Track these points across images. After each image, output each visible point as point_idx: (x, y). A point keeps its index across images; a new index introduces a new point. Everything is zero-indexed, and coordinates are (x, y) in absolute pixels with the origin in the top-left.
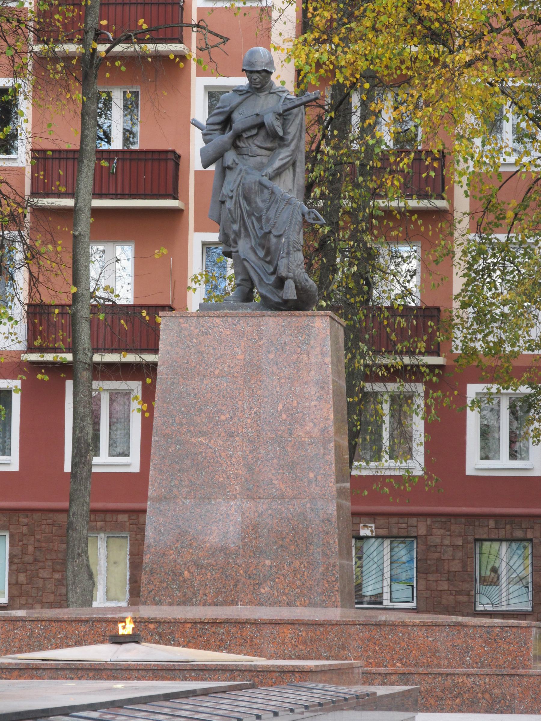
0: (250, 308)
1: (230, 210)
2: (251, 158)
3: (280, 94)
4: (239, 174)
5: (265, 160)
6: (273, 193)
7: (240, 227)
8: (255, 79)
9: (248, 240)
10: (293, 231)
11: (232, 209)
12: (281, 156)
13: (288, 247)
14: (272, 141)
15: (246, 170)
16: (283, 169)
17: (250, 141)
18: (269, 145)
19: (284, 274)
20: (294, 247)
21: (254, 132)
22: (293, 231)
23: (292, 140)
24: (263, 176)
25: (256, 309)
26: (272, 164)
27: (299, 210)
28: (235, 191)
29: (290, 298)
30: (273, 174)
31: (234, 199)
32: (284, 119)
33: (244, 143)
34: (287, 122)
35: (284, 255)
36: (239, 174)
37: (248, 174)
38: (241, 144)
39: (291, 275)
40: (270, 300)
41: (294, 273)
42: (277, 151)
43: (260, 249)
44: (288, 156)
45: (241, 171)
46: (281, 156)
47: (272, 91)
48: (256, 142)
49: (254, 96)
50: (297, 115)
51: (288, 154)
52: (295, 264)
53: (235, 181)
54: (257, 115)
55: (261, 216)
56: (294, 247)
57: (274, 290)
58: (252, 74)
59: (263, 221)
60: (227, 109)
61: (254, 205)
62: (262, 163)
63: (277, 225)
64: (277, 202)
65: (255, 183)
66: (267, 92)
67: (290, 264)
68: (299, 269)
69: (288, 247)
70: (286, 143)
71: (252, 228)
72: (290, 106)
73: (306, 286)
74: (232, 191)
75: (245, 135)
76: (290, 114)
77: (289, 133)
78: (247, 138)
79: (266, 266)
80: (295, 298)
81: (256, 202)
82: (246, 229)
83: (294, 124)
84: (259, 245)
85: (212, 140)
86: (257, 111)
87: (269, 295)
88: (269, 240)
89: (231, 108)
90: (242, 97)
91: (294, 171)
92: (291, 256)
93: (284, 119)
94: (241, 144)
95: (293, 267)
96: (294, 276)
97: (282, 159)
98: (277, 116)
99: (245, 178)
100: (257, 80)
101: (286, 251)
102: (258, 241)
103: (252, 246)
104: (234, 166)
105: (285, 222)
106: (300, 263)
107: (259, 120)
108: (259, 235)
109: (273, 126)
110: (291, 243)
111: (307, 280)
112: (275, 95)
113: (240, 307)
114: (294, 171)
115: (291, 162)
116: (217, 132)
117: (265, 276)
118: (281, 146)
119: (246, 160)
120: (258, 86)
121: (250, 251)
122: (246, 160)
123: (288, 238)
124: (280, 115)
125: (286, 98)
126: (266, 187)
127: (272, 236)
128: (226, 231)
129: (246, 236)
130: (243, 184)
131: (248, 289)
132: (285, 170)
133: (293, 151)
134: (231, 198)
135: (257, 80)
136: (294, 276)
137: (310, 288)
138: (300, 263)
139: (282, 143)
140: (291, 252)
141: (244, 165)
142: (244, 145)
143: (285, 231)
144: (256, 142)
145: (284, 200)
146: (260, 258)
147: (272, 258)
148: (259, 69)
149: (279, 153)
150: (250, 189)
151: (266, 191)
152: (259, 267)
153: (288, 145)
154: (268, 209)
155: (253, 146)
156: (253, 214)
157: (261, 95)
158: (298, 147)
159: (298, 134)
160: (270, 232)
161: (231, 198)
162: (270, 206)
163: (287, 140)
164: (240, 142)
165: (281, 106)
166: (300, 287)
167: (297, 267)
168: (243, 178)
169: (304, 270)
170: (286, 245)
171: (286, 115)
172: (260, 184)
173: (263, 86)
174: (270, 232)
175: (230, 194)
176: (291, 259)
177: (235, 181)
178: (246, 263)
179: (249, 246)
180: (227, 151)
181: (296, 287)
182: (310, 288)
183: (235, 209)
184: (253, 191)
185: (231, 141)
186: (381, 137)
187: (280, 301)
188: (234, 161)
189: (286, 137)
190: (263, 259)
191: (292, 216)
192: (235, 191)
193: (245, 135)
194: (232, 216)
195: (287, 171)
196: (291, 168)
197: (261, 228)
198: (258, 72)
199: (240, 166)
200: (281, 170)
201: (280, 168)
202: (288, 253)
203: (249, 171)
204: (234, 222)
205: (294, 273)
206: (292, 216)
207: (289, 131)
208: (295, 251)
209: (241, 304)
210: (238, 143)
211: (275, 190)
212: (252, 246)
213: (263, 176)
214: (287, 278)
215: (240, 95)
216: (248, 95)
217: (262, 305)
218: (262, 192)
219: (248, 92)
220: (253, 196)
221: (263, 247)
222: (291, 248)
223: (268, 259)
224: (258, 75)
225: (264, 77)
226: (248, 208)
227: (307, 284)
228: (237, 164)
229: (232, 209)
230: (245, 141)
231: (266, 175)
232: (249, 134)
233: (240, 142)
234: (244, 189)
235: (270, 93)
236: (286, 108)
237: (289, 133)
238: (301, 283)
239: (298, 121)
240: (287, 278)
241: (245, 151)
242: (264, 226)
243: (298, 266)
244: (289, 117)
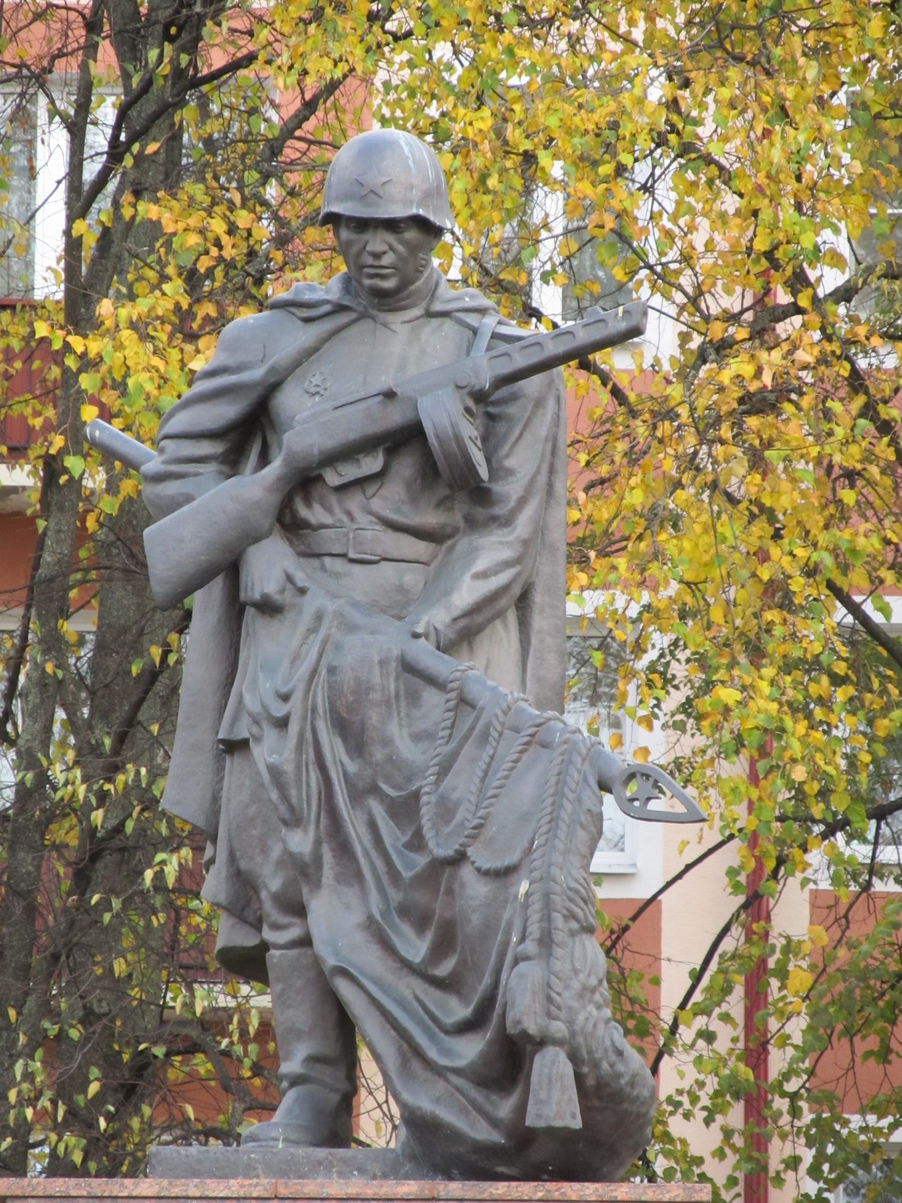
0: (362, 1171)
1: (275, 772)
2: (358, 569)
3: (472, 319)
4: (313, 630)
5: (412, 577)
6: (464, 702)
7: (318, 843)
8: (377, 256)
9: (351, 894)
10: (567, 852)
11: (289, 767)
12: (480, 565)
13: (547, 918)
14: (439, 504)
15: (339, 614)
16: (487, 613)
17: (354, 502)
18: (431, 519)
19: (532, 1027)
20: (571, 916)
21: (372, 464)
22: (567, 852)
23: (522, 502)
24: (416, 636)
25: (385, 1176)
26: (448, 593)
27: (586, 768)
28: (297, 697)
29: (558, 1123)
30: (452, 636)
31: (294, 728)
32: (491, 417)
33: (329, 510)
34: (501, 428)
35: (530, 947)
36: (313, 630)
37: (350, 628)
38: (314, 514)
39: (558, 1028)
40: (456, 1136)
41: (570, 1023)
42: (462, 544)
43: (407, 929)
44: (507, 564)
45: (319, 617)
46: (480, 565)
47: (437, 307)
48: (377, 505)
49: (365, 326)
50: (539, 403)
51: (507, 554)
52: (576, 985)
53: (295, 659)
54: (390, 395)
55: (416, 796)
56: (571, 916)
57: (475, 1093)
58: (368, 236)
59: (426, 813)
60: (256, 374)
61: (379, 754)
62: (401, 589)
63: (491, 830)
64: (485, 737)
65: (383, 663)
66: (416, 312)
67: (557, 985)
68: (591, 1008)
69: (547, 918)
70: (497, 510)
71: (369, 845)
72: (520, 361)
73: (619, 1076)
74: (285, 698)
75: (332, 478)
76: (513, 398)
77: (511, 472)
78: (341, 489)
79: (431, 996)
80: (577, 1123)
81: (387, 742)
82: (344, 849)
83: (528, 436)
84: (404, 911)
85: (189, 499)
86: (385, 381)
87: (447, 1116)
88: (450, 892)
89: (272, 370)
90: (307, 335)
91: (524, 624)
92: (558, 952)
93: (491, 417)
94: (314, 514)
95: (567, 998)
96: (573, 1034)
97: (484, 575)
98: (470, 403)
99: (338, 647)
100: (387, 260)
101: (534, 930)
102: (395, 896)
103: (370, 918)
104: (288, 597)
105: (525, 818)
106: (593, 981)
107: (395, 417)
108: (406, 874)
109: (458, 438)
110: (557, 900)
111: (620, 1053)
112: (448, 324)
113: (316, 1168)
114: (524, 624)
115: (516, 591)
116: (210, 469)
117: (432, 1037)
118: (472, 524)
119: (337, 576)
120: (389, 284)
121: (360, 937)
122: (337, 576)
123: (546, 878)
124: (480, 397)
125: (495, 336)
126: (432, 681)
127: (467, 873)
128: (243, 865)
129: (340, 879)
130: (332, 670)
131: (335, 1098)
132: (491, 620)
133: (526, 543)
134: (282, 723)
135: (387, 260)
136: (573, 1034)
137: (632, 1084)
138: (593, 981)
139: (481, 513)
140: (560, 936)
141: (335, 596)
142: (327, 519)
143: (529, 851)
144: (377, 505)
145: (517, 730)
146: (406, 965)
147: (462, 962)
148: (398, 211)
149: (473, 552)
150: (362, 689)
151: (431, 697)
152: (402, 1003)
153: (507, 521)
154: (445, 768)
155: (363, 519)
156: (374, 790)
157: (396, 319)
158: (540, 529)
159: (542, 479)
160: (461, 857)
161: (282, 723)
162: (453, 757)
163: (502, 500)
164: (308, 503)
165: (484, 363)
166: (590, 1082)
167: (581, 996)
168: (329, 647)
169: (608, 1012)
170: (536, 906)
171: (497, 403)
172: (408, 667)
173: (404, 285)
174: (461, 857)
175: (279, 710)
176: (557, 965)
177: (295, 659)
178: (344, 988)
179: (357, 917)
180: (255, 538)
181: (579, 1078)
182: (632, 1084)
183: (298, 767)
184: (376, 696)
185: (275, 500)
186: (357, 679)
187: (496, 1137)
188: (290, 579)
189: (497, 488)
190: (420, 973)
191: (559, 794)
192: (297, 697)
193: (332, 478)
194: (284, 797)
195: (498, 623)
196: (512, 616)
197: (417, 843)
198: (391, 225)
199: (309, 605)
200: (479, 619)
201: (476, 608)
202: (546, 941)
203: (358, 618)
204: (294, 820)
205: (570, 1023)
206: (559, 794)
207: (510, 463)
208: (572, 934)
209: (322, 1153)
210: (303, 512)
211: (474, 691)
212: (370, 918)
213: (416, 636)
214: (541, 1043)
215: (307, 320)
216: (343, 318)
217: (413, 1158)
218: (414, 698)
219: (340, 308)
220: (374, 717)
221: (421, 922)
222: (558, 920)
223: (444, 969)
224: (390, 238)
225: (414, 249)
226: (352, 767)
227: (620, 1067)
228: (302, 591)
229: (289, 767)
230: (333, 499)
231: (426, 636)
232: (350, 472)
233: (308, 503)
234: (334, 690)
235: (430, 314)
236: (505, 368)
237: (511, 472)
238: (596, 1065)
239: (542, 427)
240: (541, 1043)
241: (329, 540)
242: (428, 833)
243: (587, 992)
244: (511, 409)
